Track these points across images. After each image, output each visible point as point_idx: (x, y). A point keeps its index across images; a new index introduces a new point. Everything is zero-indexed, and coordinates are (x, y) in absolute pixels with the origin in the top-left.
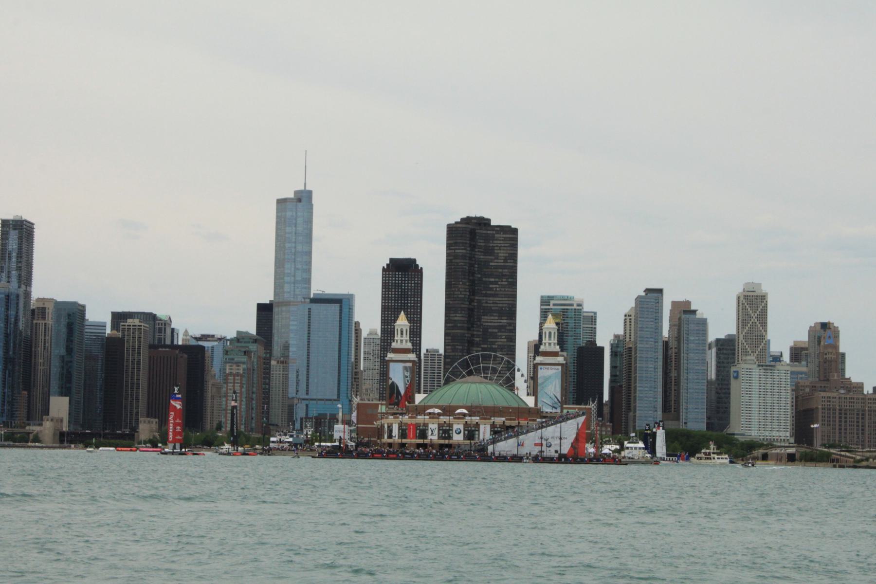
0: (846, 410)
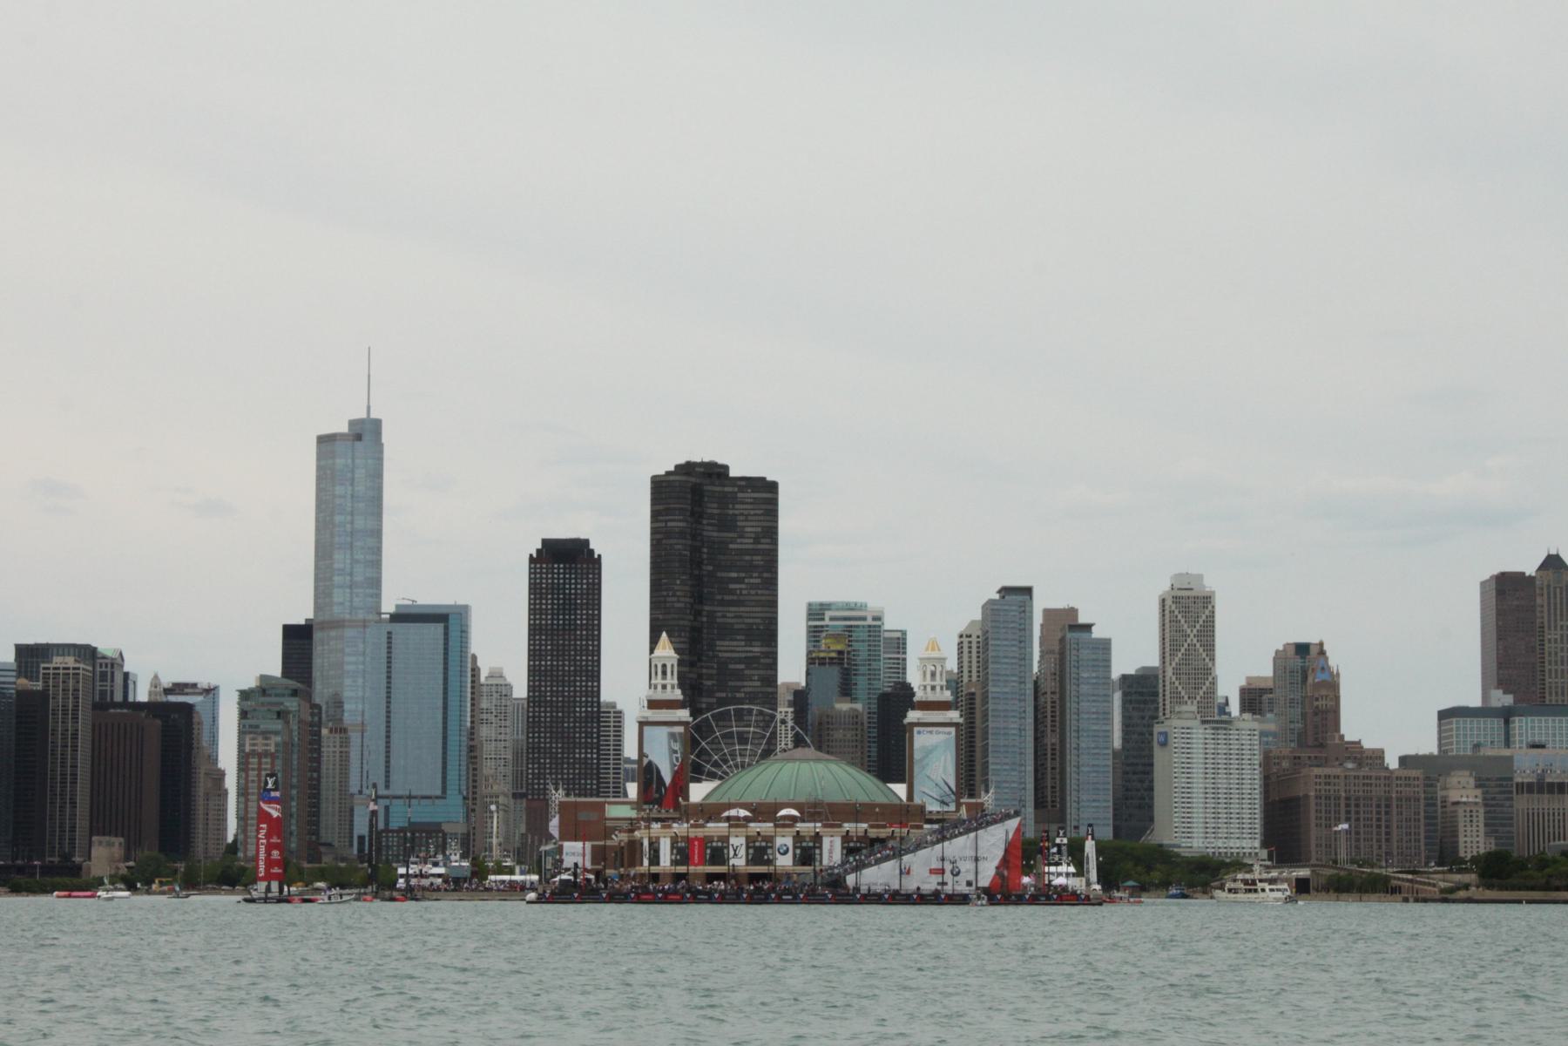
0: (1357, 799)
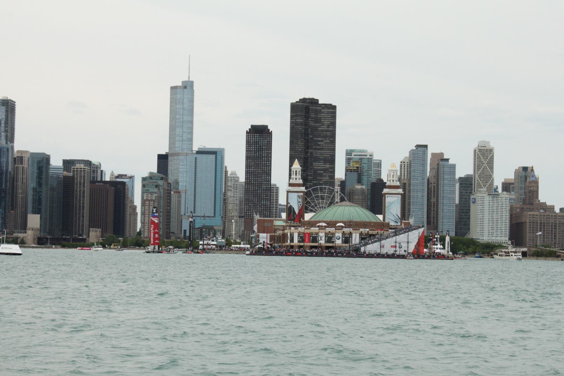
0: (544, 223)
